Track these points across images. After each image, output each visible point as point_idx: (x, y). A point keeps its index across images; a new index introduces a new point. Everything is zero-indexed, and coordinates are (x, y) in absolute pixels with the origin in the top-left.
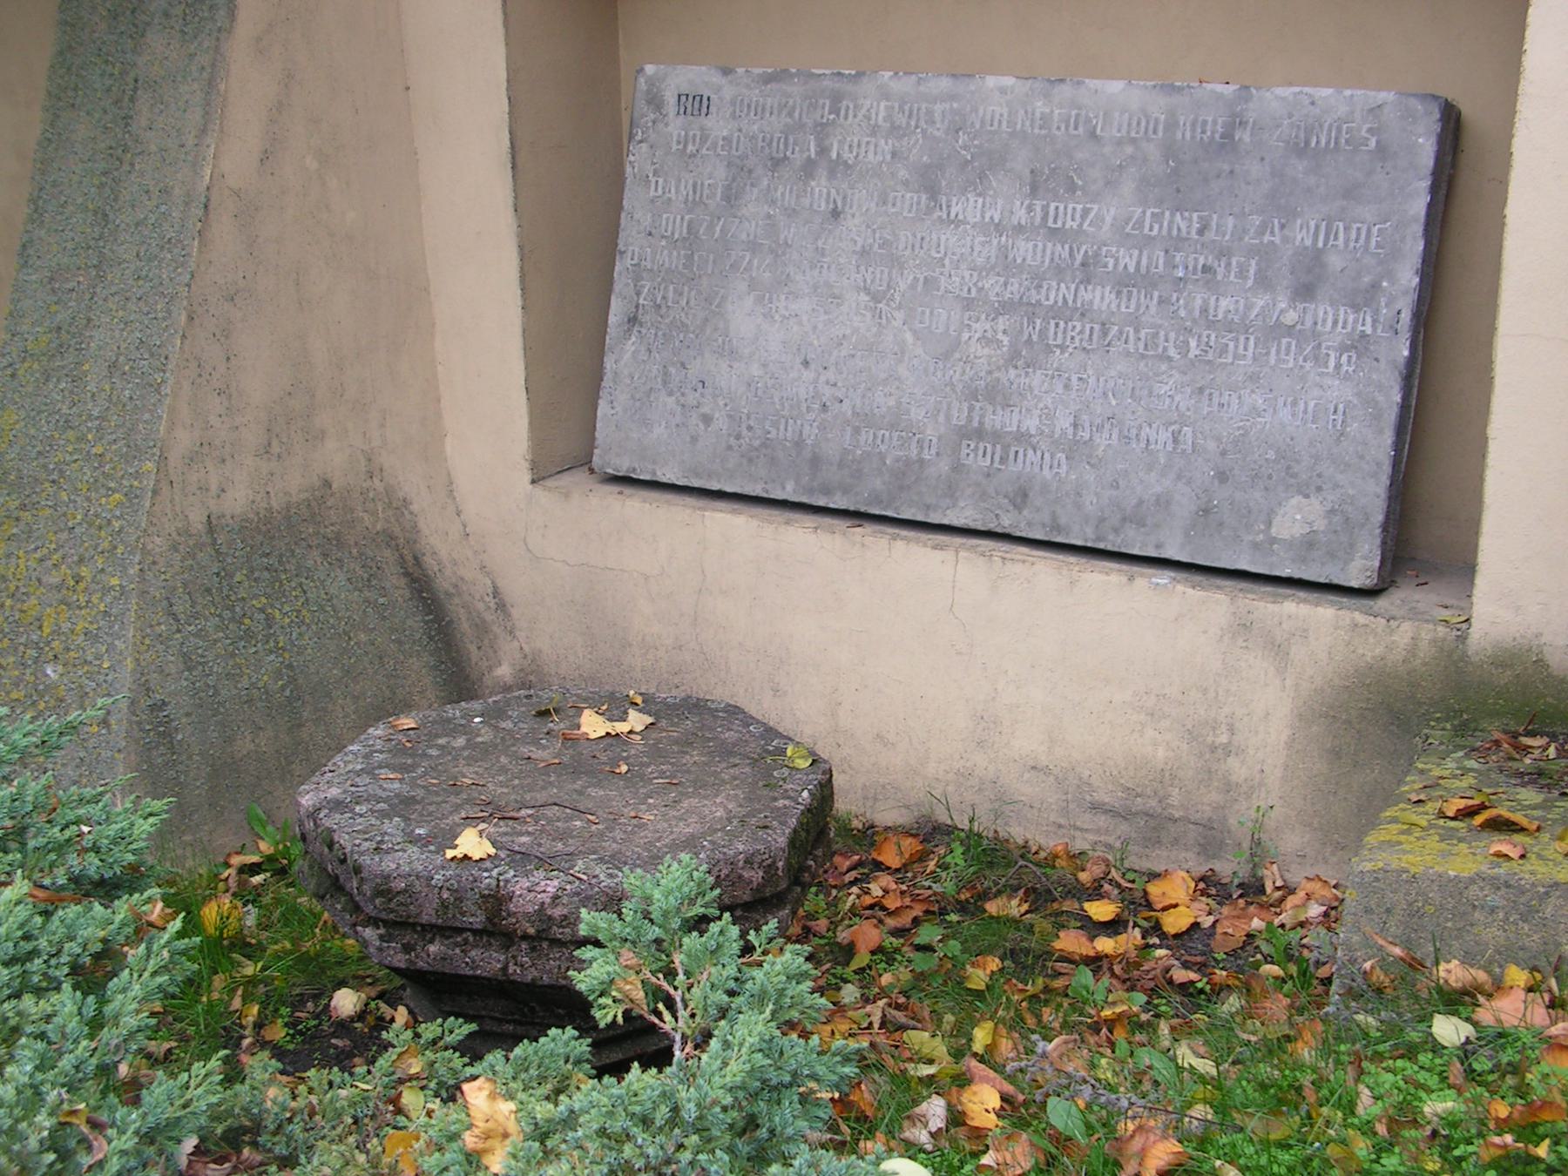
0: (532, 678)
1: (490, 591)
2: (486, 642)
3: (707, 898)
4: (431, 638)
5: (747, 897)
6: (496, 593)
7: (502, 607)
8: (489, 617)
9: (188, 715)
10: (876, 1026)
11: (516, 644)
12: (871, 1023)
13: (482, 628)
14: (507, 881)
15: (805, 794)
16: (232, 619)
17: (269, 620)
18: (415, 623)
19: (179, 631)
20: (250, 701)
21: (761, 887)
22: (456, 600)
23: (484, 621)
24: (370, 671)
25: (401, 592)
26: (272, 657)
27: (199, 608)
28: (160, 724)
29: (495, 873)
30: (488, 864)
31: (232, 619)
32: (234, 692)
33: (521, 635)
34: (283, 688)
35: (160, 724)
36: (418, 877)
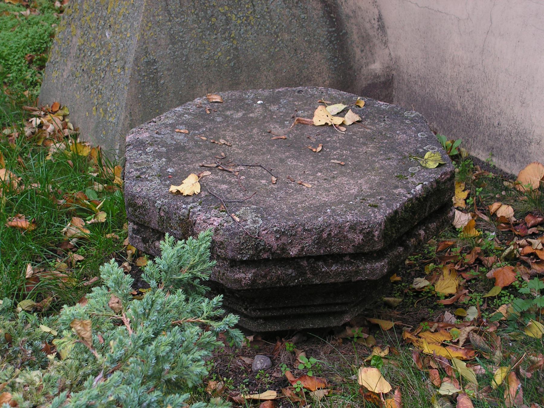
0: (394, 72)
1: (376, 17)
2: (367, 48)
3: (205, 266)
4: (331, 42)
5: (350, 250)
6: (380, 19)
7: (382, 28)
8: (372, 33)
9: (169, 70)
10: (461, 343)
11: (387, 51)
12: (458, 341)
13: (366, 39)
14: (194, 213)
15: (419, 187)
16: (205, 18)
17: (228, 21)
18: (322, 32)
19: (170, 21)
20: (208, 66)
21: (359, 246)
22: (353, 21)
23: (368, 35)
24: (288, 57)
25: (317, 12)
26: (226, 42)
27: (184, 8)
28: (152, 73)
29: (189, 206)
30: (191, 199)
31: (205, 18)
32: (198, 60)
33: (391, 46)
34: (230, 61)
35: (152, 73)
36: (149, 200)
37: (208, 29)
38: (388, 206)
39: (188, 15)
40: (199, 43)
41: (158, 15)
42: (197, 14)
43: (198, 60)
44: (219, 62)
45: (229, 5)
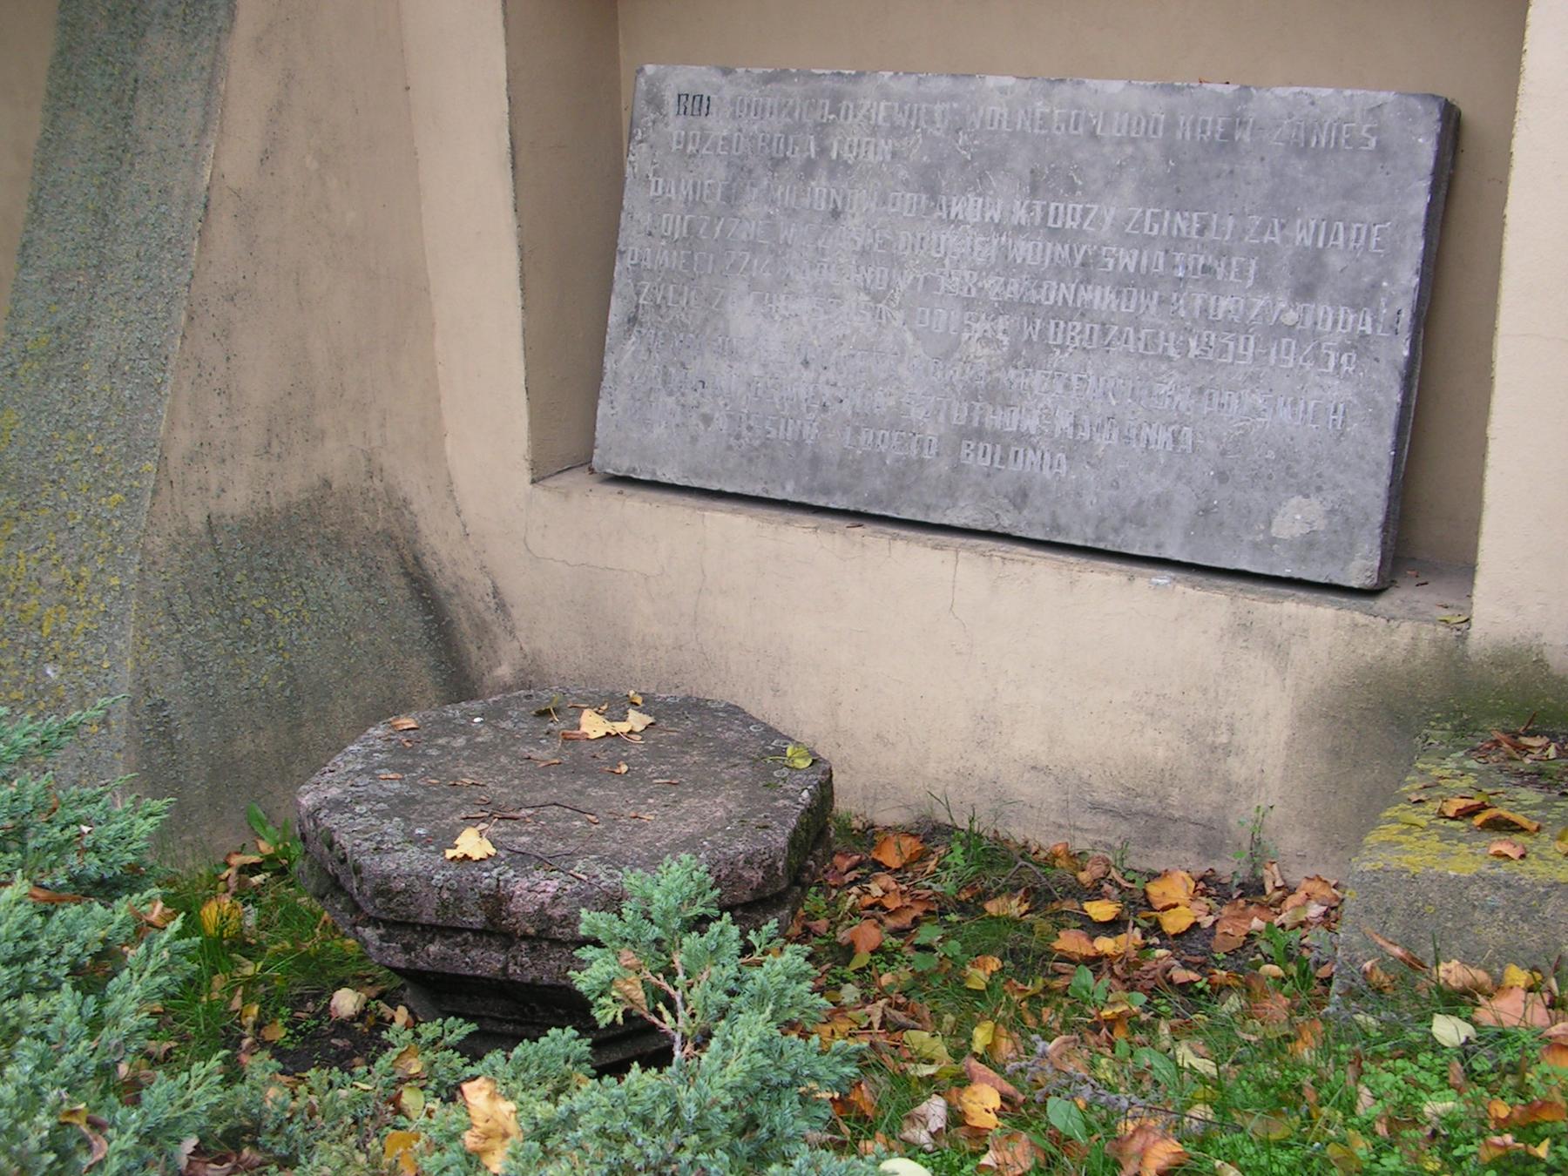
0: (532, 678)
1: (490, 591)
2: (486, 642)
3: (707, 898)
4: (431, 638)
5: (747, 897)
6: (496, 593)
7: (502, 607)
8: (489, 617)
9: (188, 715)
10: (876, 1026)
11: (516, 644)
12: (871, 1023)
13: (482, 628)
14: (507, 881)
15: (805, 794)
16: (232, 619)
17: (269, 620)
18: (415, 623)
19: (179, 631)
20: (250, 701)
21: (761, 887)
22: (456, 600)
23: (484, 621)
25: (401, 592)
26: (272, 657)
27: (199, 608)
28: (160, 724)
30: (488, 864)
31: (232, 619)
32: (234, 692)
33: (521, 635)
34: (283, 688)
35: (160, 724)
36: (418, 877)
37: (241, 638)
38: (783, 823)
39: (206, 620)
40: (231, 663)
41: (159, 624)
42: (220, 616)
43: (234, 692)
44: (267, 693)
45: (268, 596)
